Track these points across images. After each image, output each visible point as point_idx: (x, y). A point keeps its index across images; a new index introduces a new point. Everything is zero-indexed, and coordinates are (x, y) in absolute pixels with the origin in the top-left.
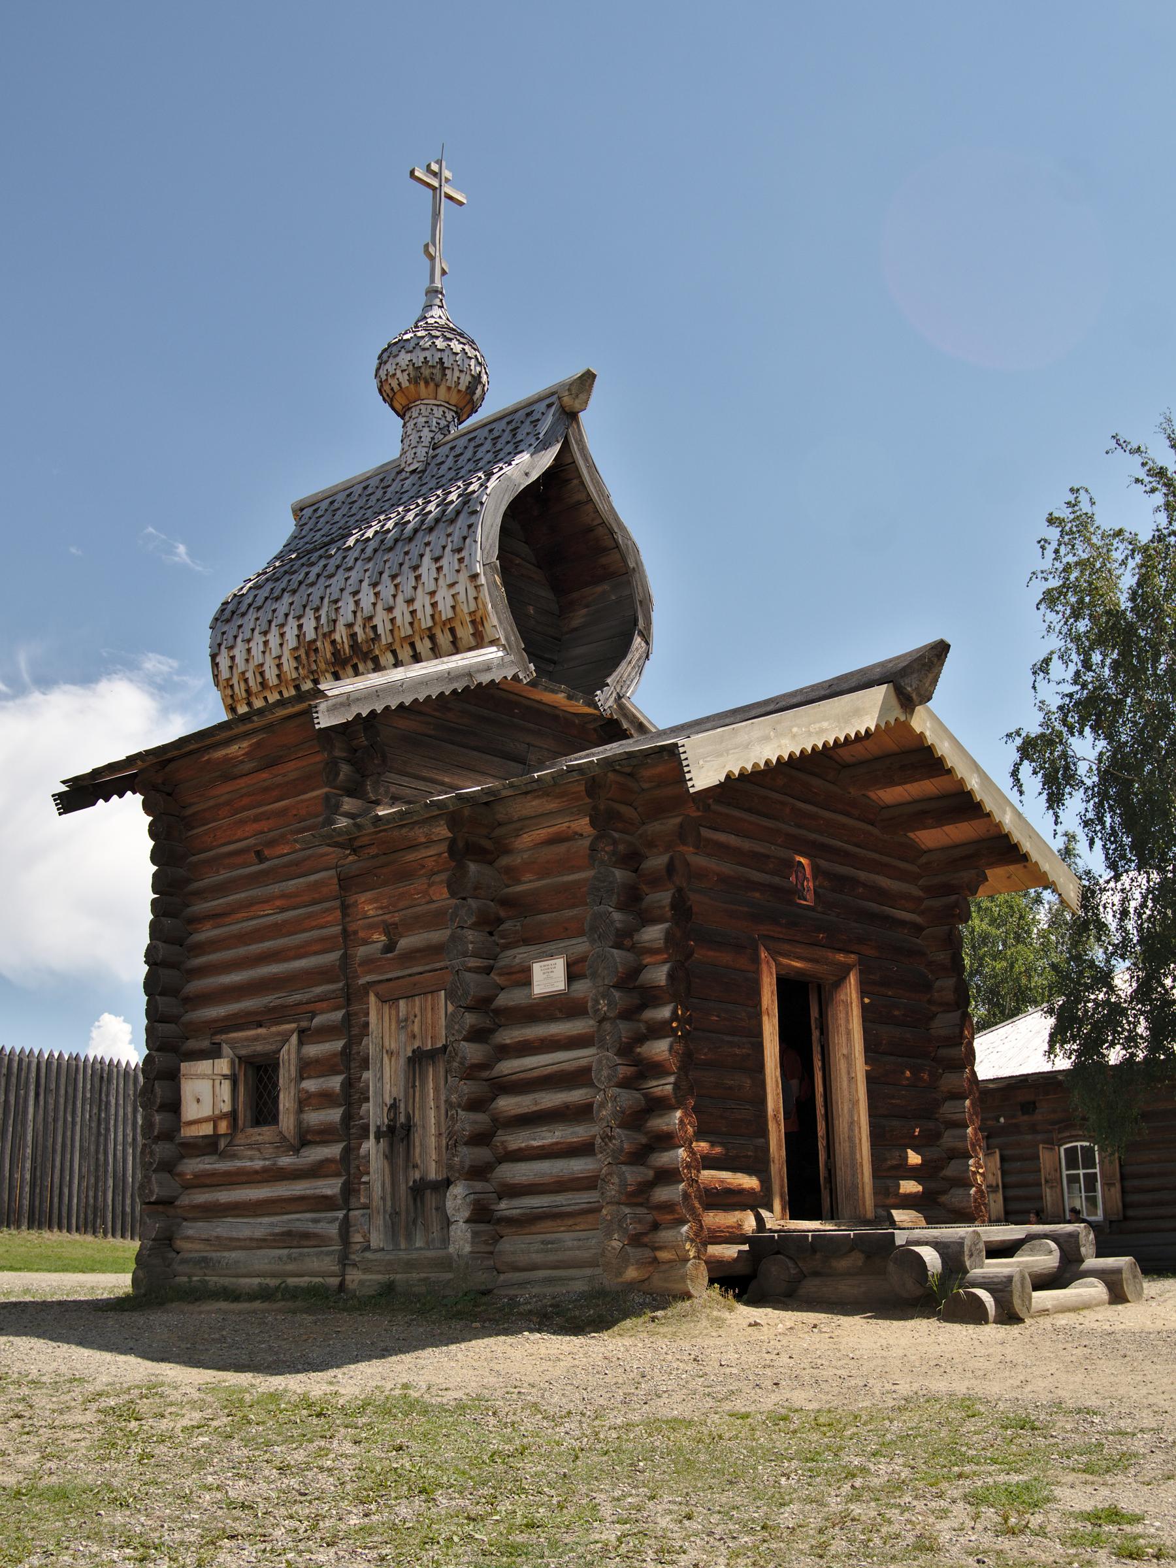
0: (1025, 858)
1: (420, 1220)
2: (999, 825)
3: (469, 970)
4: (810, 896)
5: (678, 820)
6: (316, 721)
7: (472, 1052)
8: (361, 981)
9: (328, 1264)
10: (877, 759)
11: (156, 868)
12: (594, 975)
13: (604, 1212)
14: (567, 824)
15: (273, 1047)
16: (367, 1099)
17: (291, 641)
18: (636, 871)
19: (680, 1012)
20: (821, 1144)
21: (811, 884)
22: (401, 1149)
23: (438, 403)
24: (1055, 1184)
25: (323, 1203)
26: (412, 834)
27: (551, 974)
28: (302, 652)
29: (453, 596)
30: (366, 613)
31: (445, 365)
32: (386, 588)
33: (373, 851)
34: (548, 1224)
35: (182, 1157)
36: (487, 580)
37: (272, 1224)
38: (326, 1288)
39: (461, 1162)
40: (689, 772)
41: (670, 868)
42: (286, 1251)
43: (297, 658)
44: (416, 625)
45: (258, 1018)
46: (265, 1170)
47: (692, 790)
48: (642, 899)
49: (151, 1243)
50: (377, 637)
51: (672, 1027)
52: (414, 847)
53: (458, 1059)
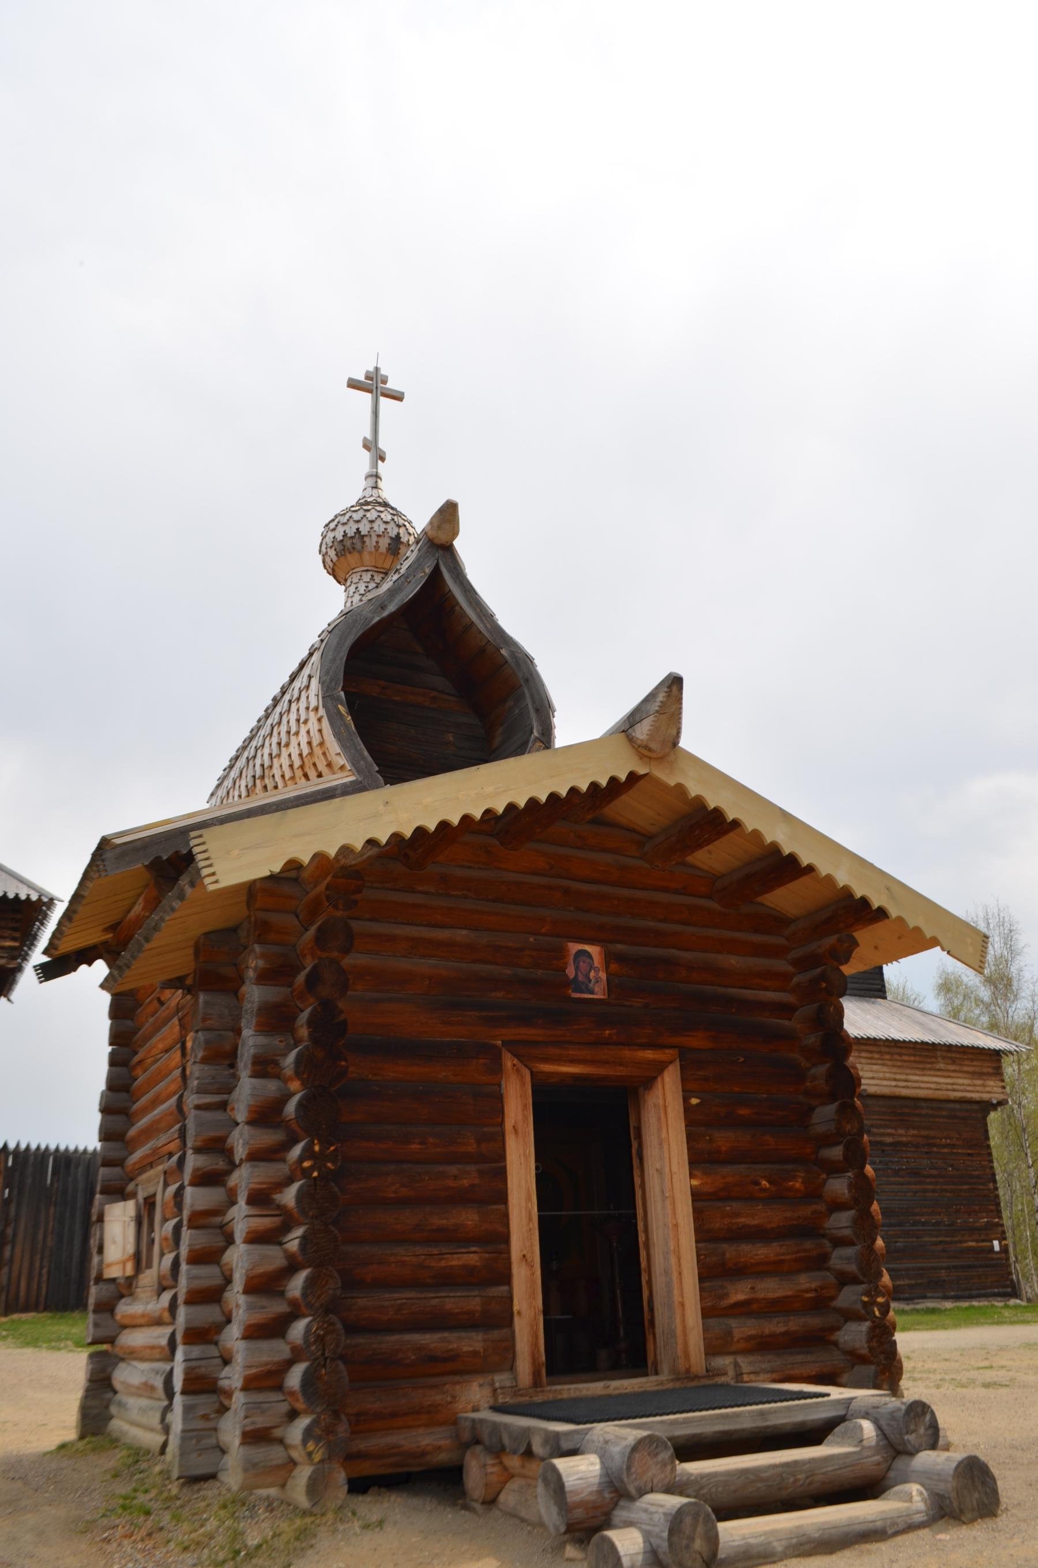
0: (881, 914)
19: (317, 1148)
21: (603, 975)
23: (366, 568)
31: (362, 534)
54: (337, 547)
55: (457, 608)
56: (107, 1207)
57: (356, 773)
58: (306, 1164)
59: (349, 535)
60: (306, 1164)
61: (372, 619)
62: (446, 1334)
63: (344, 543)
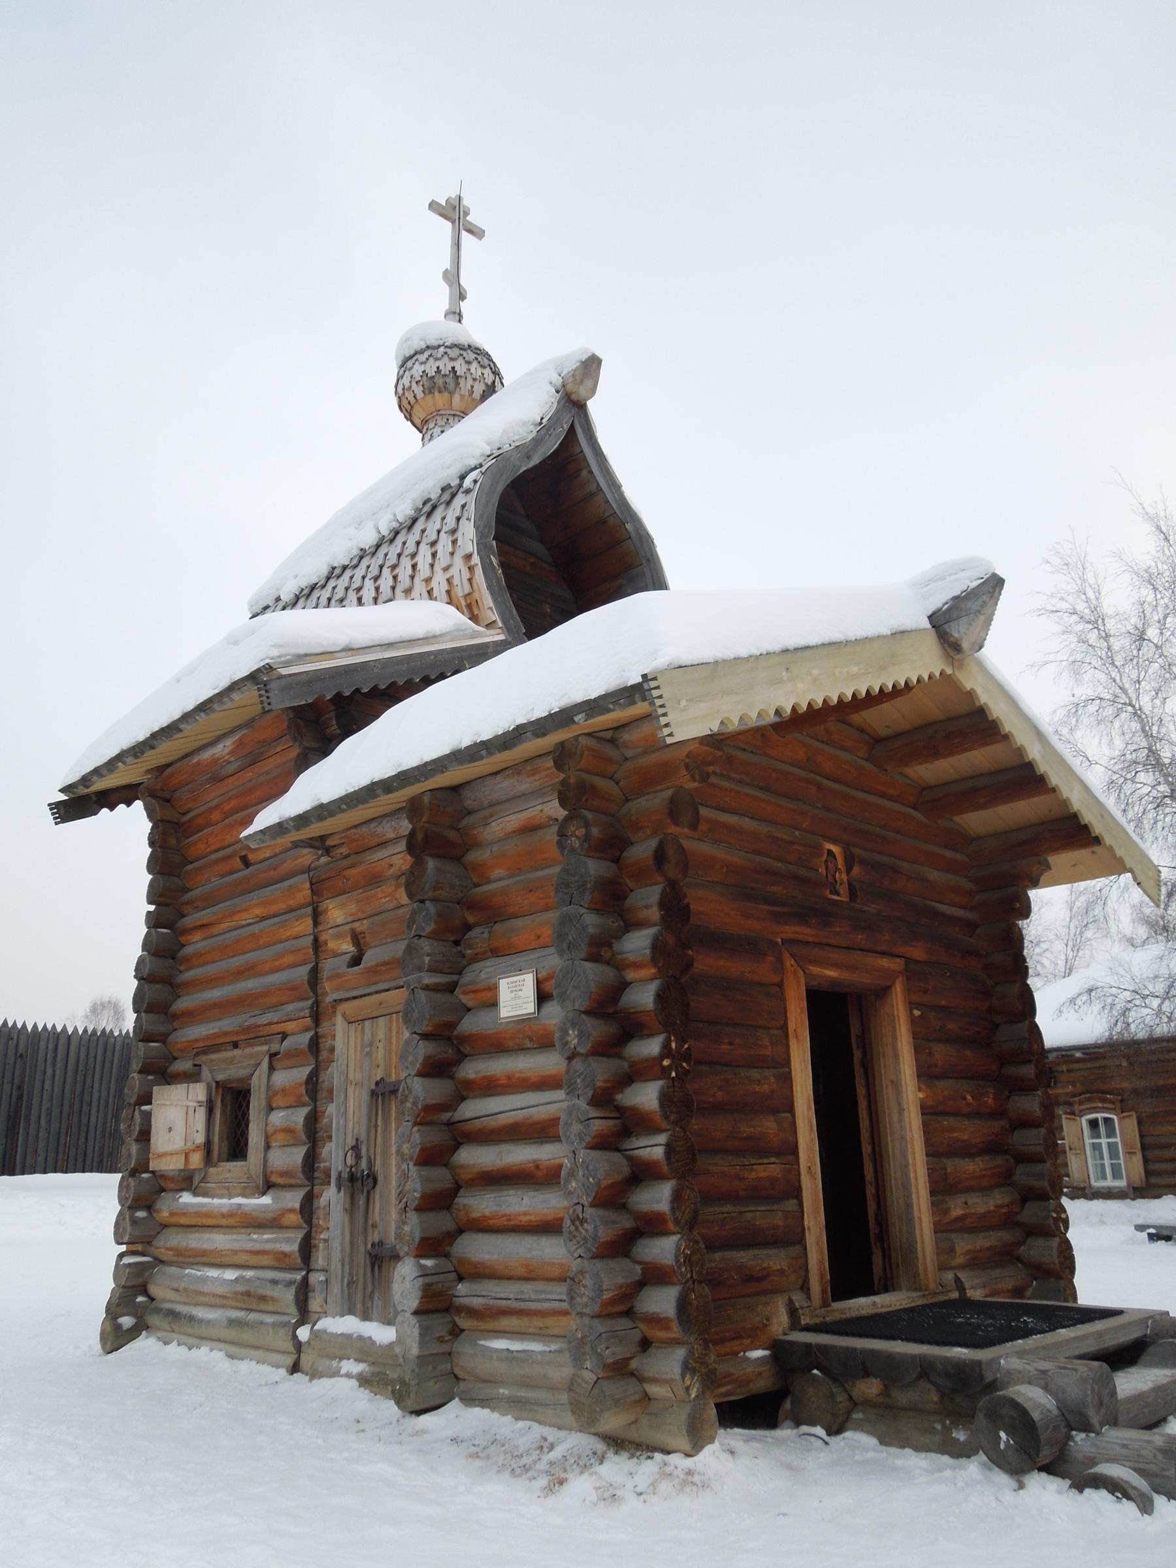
0: (1097, 841)
2: (1065, 803)
4: (843, 890)
5: (669, 792)
10: (917, 729)
11: (151, 877)
12: (563, 998)
14: (538, 807)
18: (616, 861)
19: (673, 1045)
20: (870, 1190)
21: (845, 877)
23: (453, 413)
24: (1078, 1152)
26: (379, 830)
27: (520, 993)
33: (344, 850)
39: (411, 1232)
40: (665, 715)
41: (660, 856)
45: (234, 1039)
48: (625, 898)
51: (663, 1068)
52: (382, 845)
53: (411, 1100)
54: (425, 383)
55: (584, 472)
56: (155, 1088)
57: (506, 633)
58: (666, 1063)
59: (443, 373)
60: (666, 1063)
61: (520, 467)
62: (756, 1252)
63: (436, 380)
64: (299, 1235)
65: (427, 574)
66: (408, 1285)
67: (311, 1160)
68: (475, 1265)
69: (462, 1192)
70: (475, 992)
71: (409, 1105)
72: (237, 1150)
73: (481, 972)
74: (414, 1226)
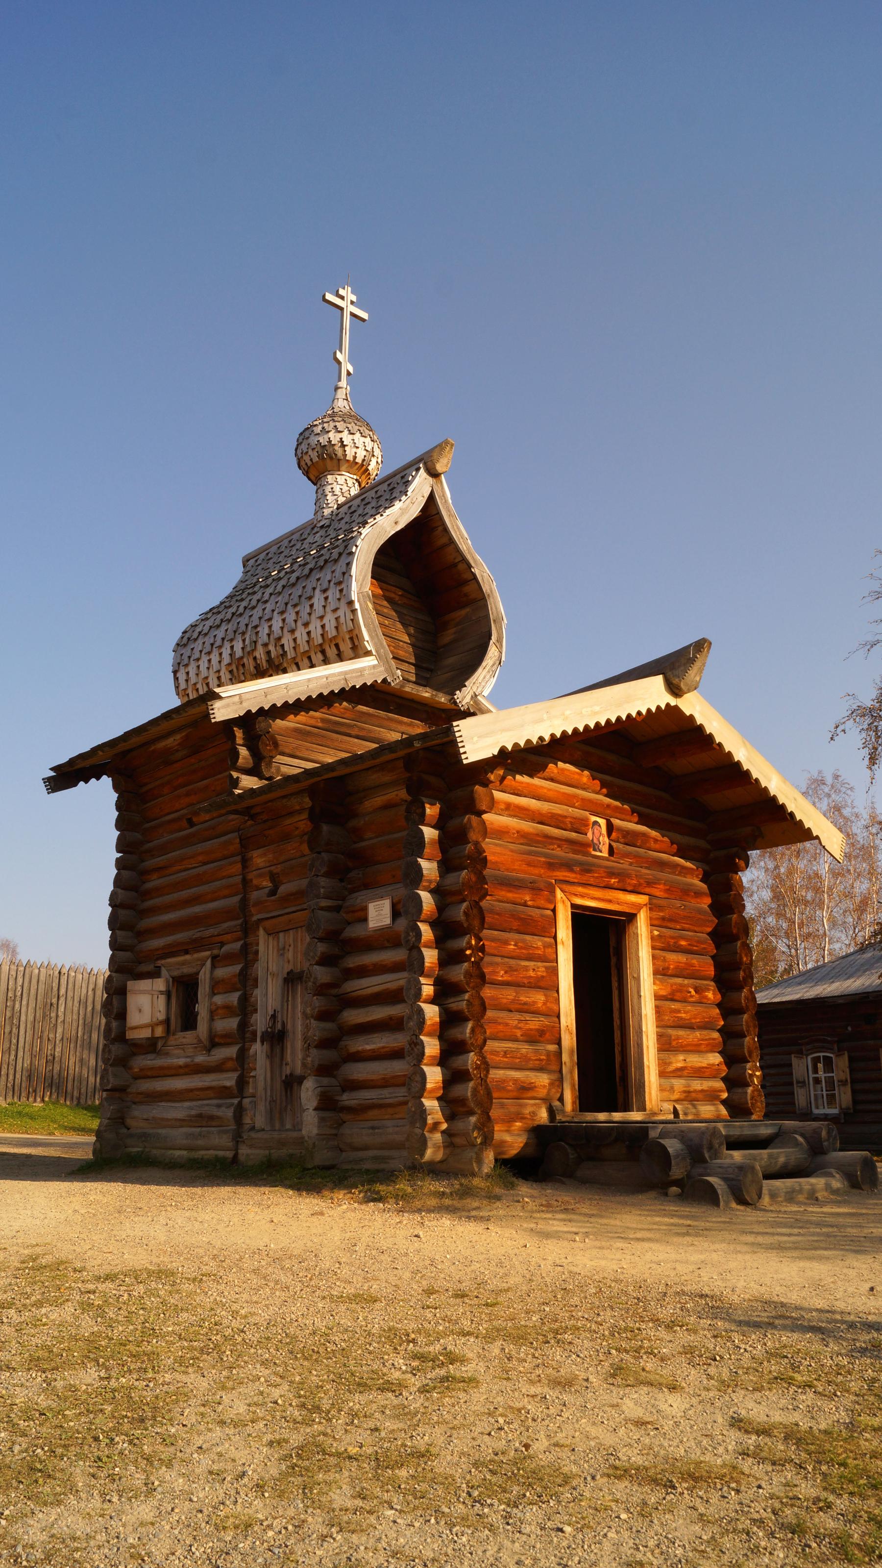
1: (289, 1107)
3: (322, 909)
6: (212, 716)
7: (322, 974)
8: (255, 918)
9: (225, 1140)
13: (410, 1104)
14: (395, 793)
15: (194, 970)
16: (256, 1011)
17: (226, 659)
19: (473, 942)
20: (617, 1050)
22: (278, 1050)
25: (223, 1092)
28: (234, 667)
29: (336, 619)
30: (276, 636)
32: (290, 616)
34: (375, 1113)
35: (134, 1054)
36: (360, 605)
37: (191, 1108)
38: (224, 1159)
42: (199, 1129)
43: (231, 672)
44: (311, 643)
46: (186, 1066)
47: (465, 762)
49: (107, 1121)
50: (284, 654)
52: (291, 814)
64: (235, 1075)
65: (321, 613)
66: (310, 1093)
67: (243, 1025)
68: (353, 1081)
69: (345, 1038)
70: (353, 912)
71: (310, 984)
72: (189, 1021)
73: (358, 898)
74: (316, 1056)
